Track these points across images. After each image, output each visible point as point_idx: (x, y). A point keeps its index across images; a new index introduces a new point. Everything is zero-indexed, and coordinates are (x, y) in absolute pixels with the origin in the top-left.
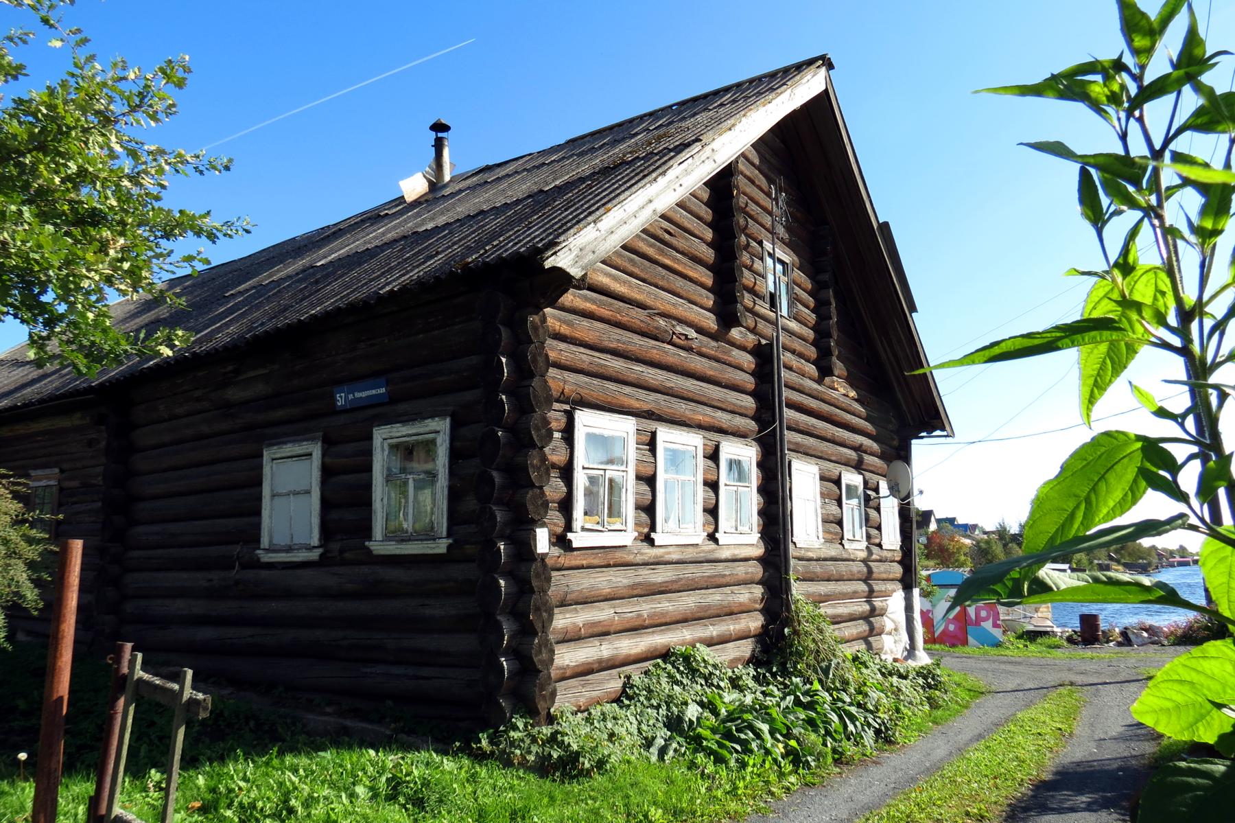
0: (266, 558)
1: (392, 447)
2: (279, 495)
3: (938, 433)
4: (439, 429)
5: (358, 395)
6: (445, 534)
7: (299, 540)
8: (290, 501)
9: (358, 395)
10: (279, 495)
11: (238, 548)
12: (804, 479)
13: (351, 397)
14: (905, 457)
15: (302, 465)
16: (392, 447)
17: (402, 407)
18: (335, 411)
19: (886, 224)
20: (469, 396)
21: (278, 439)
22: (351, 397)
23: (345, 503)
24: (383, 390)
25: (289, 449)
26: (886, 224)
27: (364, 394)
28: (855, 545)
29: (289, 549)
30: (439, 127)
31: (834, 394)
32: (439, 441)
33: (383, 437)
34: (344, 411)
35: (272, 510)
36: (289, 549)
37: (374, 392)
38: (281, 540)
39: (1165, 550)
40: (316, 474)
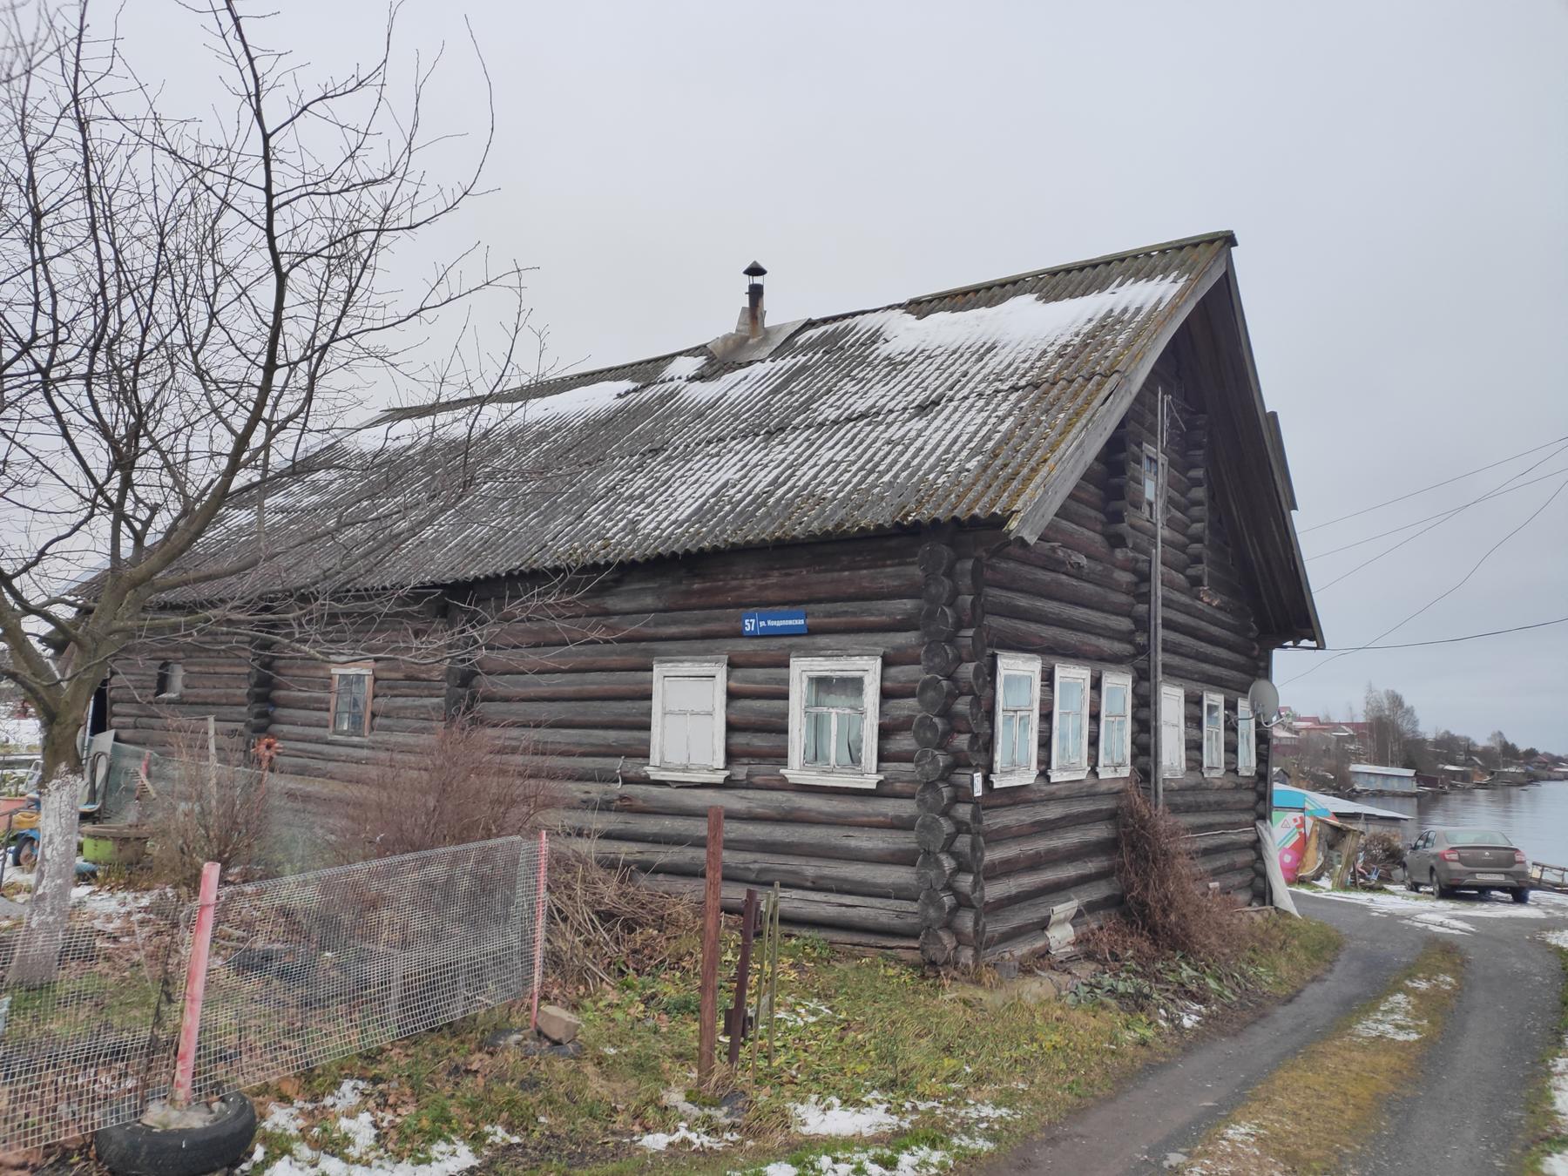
0: (656, 775)
1: (811, 679)
2: (671, 713)
3: (1305, 643)
4: (869, 669)
5: (770, 623)
6: (874, 770)
7: (697, 760)
8: (687, 718)
9: (770, 623)
10: (671, 713)
11: (620, 761)
12: (1171, 702)
13: (762, 624)
14: (1265, 672)
15: (707, 684)
16: (811, 679)
17: (822, 640)
18: (739, 634)
19: (1274, 415)
20: (902, 639)
21: (668, 656)
22: (762, 624)
23: (754, 732)
24: (801, 622)
25: (687, 668)
26: (1274, 415)
27: (779, 623)
28: (1214, 774)
29: (686, 769)
30: (755, 271)
31: (1199, 604)
32: (867, 681)
33: (801, 670)
34: (753, 636)
35: (663, 727)
36: (686, 769)
37: (790, 622)
38: (675, 758)
39: (1547, 755)
40: (721, 698)
